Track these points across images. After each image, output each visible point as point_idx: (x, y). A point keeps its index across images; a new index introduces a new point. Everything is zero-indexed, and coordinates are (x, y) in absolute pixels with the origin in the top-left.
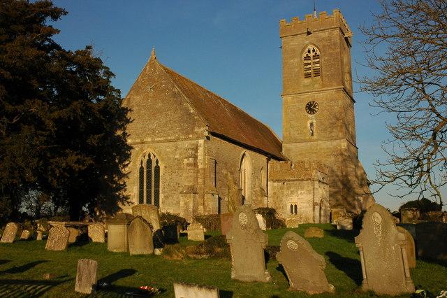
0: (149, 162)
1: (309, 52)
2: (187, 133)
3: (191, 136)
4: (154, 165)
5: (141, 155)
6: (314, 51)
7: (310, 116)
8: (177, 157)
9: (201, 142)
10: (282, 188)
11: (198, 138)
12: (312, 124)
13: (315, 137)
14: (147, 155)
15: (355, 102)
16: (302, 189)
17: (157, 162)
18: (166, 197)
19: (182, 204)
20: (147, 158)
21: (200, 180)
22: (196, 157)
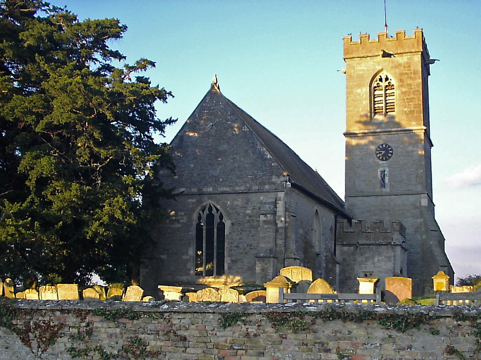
0: (210, 217)
1: (381, 80)
2: (263, 184)
3: (267, 187)
4: (217, 220)
5: (199, 208)
6: (387, 79)
7: (381, 162)
8: (249, 212)
9: (281, 195)
10: (353, 254)
11: (276, 190)
12: (383, 172)
13: (387, 190)
14: (207, 209)
15: (433, 146)
16: (380, 255)
17: (221, 217)
18: (234, 262)
19: (258, 269)
20: (207, 211)
21: (280, 242)
22: (275, 213)
